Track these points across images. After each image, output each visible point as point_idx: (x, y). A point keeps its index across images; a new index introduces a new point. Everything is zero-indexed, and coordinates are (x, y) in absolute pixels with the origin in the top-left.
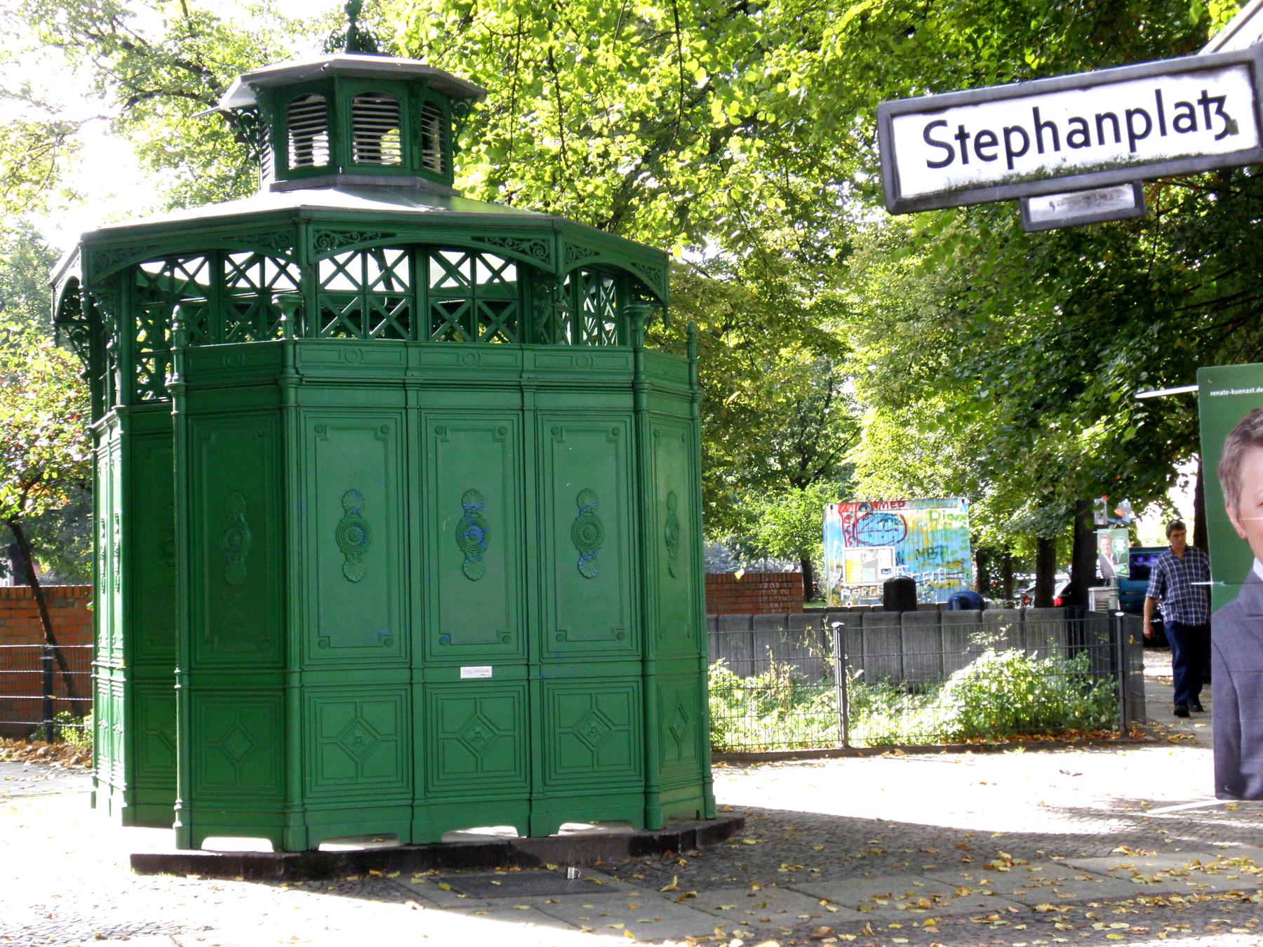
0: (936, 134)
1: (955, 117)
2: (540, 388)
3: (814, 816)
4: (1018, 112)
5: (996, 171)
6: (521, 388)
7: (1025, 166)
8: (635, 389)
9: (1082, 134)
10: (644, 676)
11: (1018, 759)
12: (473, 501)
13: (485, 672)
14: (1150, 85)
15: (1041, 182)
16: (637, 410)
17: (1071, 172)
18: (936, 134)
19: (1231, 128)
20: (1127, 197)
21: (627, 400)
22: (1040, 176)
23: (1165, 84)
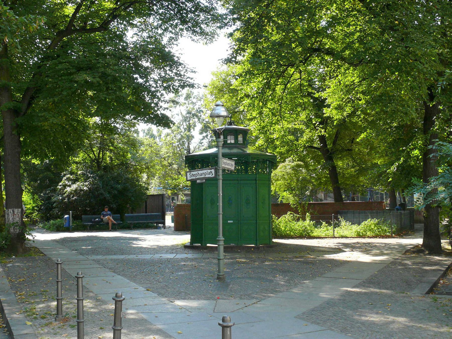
0: (190, 174)
1: (192, 173)
2: (241, 180)
3: (82, 237)
4: (196, 172)
5: (195, 178)
6: (238, 180)
7: (197, 177)
8: (256, 180)
9: (201, 175)
10: (256, 223)
11: (370, 242)
12: (230, 197)
13: (232, 222)
14: (206, 170)
15: (198, 179)
16: (256, 183)
17: (200, 178)
18: (190, 174)
19: (212, 175)
20: (204, 181)
21: (254, 182)
22: (198, 178)
23: (208, 170)
